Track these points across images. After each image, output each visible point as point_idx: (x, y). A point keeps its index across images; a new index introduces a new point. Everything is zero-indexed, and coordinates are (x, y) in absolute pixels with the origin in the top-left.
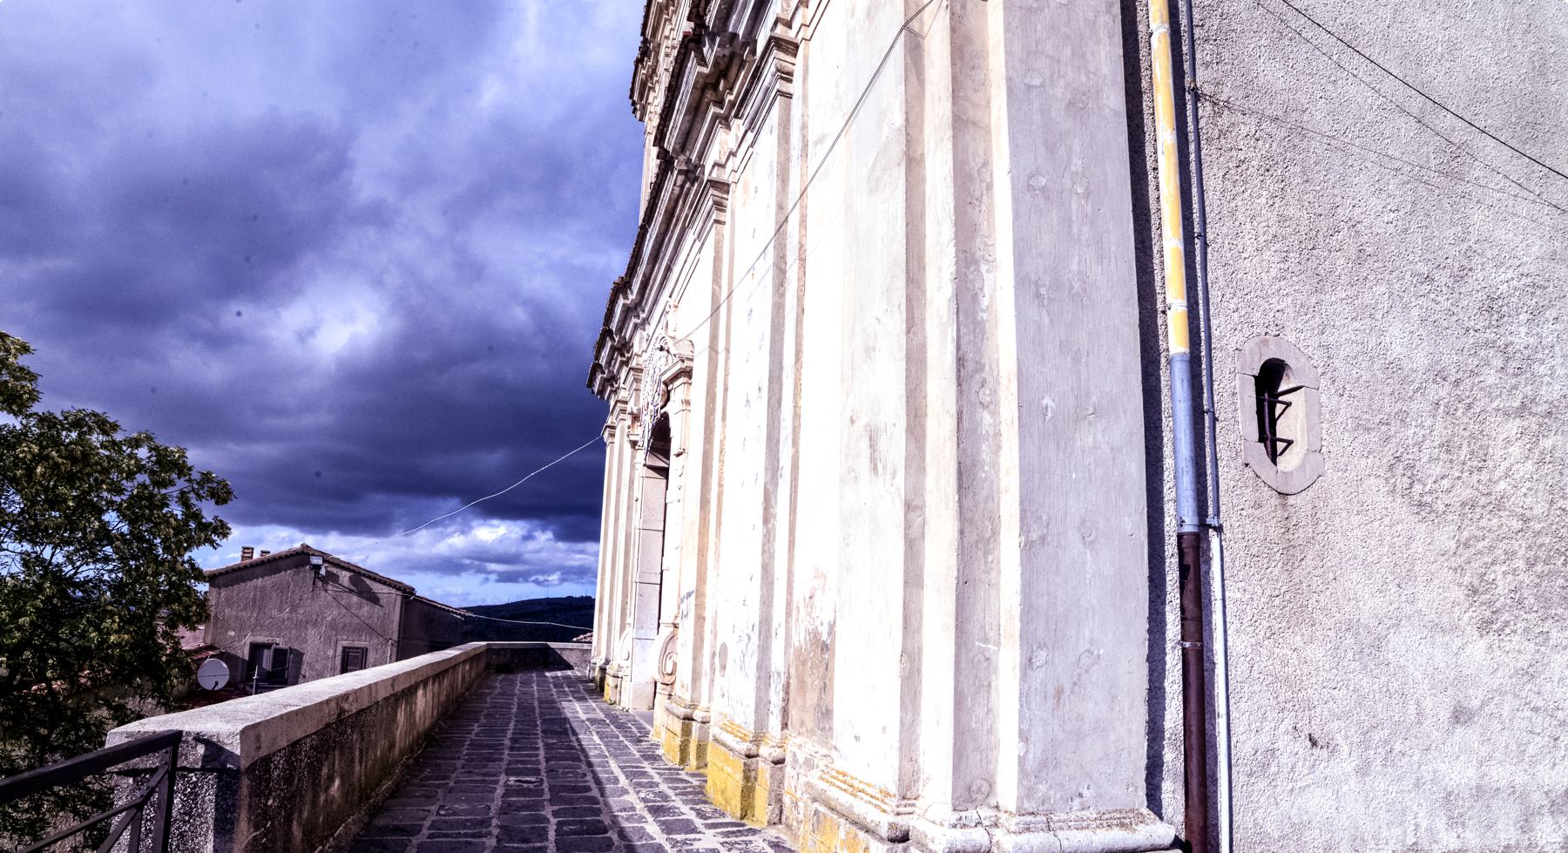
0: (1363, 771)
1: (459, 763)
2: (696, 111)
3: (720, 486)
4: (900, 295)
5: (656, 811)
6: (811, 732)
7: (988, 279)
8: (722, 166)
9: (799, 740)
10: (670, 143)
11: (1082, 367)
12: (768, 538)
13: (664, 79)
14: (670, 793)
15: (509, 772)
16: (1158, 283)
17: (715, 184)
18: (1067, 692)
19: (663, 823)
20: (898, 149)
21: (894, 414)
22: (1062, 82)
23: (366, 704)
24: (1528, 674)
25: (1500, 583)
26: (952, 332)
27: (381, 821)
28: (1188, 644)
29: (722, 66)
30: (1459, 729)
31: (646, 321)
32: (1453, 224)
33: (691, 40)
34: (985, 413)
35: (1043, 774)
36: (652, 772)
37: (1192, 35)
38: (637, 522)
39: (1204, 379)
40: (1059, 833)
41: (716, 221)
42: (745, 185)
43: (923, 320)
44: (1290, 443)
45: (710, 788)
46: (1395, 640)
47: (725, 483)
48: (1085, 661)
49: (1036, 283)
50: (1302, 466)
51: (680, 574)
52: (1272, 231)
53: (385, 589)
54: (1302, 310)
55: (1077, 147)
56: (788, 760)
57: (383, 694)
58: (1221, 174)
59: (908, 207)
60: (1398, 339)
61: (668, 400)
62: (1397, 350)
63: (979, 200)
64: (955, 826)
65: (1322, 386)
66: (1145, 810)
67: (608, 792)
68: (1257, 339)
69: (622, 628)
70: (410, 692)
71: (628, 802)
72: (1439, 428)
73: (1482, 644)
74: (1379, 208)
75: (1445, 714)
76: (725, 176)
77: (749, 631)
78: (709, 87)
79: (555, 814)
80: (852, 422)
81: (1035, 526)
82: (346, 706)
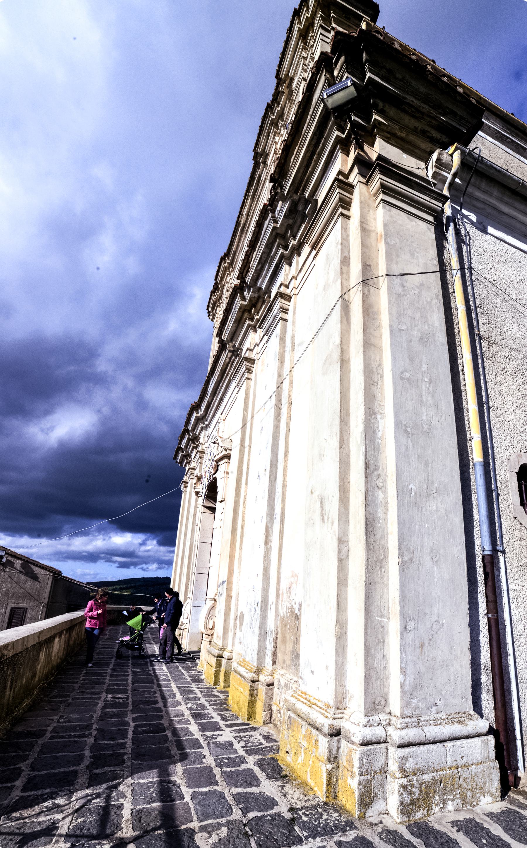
1: (77, 686)
2: (239, 322)
3: (243, 521)
4: (336, 428)
5: (196, 716)
6: (289, 667)
8: (252, 350)
9: (282, 672)
10: (225, 336)
11: (430, 469)
13: (224, 306)
14: (207, 704)
15: (108, 692)
17: (247, 359)
18: (426, 645)
19: (200, 724)
20: (336, 355)
22: (416, 329)
23: (19, 650)
27: (19, 729)
28: (490, 616)
29: (254, 302)
31: (208, 426)
33: (238, 288)
34: (380, 492)
35: (415, 693)
36: (197, 691)
37: (476, 311)
38: (196, 538)
39: (492, 474)
40: (425, 728)
41: (247, 378)
42: (263, 362)
43: (348, 442)
45: (231, 702)
47: (246, 519)
48: (435, 627)
49: (405, 425)
51: (218, 571)
52: (520, 401)
53: (43, 572)
55: (424, 360)
56: (276, 684)
57: (32, 643)
58: (494, 374)
61: (217, 470)
64: (366, 726)
66: (472, 712)
68: (516, 454)
70: (51, 640)
76: (252, 355)
77: (255, 606)
78: (246, 312)
79: (134, 720)
80: (312, 493)
82: (6, 652)
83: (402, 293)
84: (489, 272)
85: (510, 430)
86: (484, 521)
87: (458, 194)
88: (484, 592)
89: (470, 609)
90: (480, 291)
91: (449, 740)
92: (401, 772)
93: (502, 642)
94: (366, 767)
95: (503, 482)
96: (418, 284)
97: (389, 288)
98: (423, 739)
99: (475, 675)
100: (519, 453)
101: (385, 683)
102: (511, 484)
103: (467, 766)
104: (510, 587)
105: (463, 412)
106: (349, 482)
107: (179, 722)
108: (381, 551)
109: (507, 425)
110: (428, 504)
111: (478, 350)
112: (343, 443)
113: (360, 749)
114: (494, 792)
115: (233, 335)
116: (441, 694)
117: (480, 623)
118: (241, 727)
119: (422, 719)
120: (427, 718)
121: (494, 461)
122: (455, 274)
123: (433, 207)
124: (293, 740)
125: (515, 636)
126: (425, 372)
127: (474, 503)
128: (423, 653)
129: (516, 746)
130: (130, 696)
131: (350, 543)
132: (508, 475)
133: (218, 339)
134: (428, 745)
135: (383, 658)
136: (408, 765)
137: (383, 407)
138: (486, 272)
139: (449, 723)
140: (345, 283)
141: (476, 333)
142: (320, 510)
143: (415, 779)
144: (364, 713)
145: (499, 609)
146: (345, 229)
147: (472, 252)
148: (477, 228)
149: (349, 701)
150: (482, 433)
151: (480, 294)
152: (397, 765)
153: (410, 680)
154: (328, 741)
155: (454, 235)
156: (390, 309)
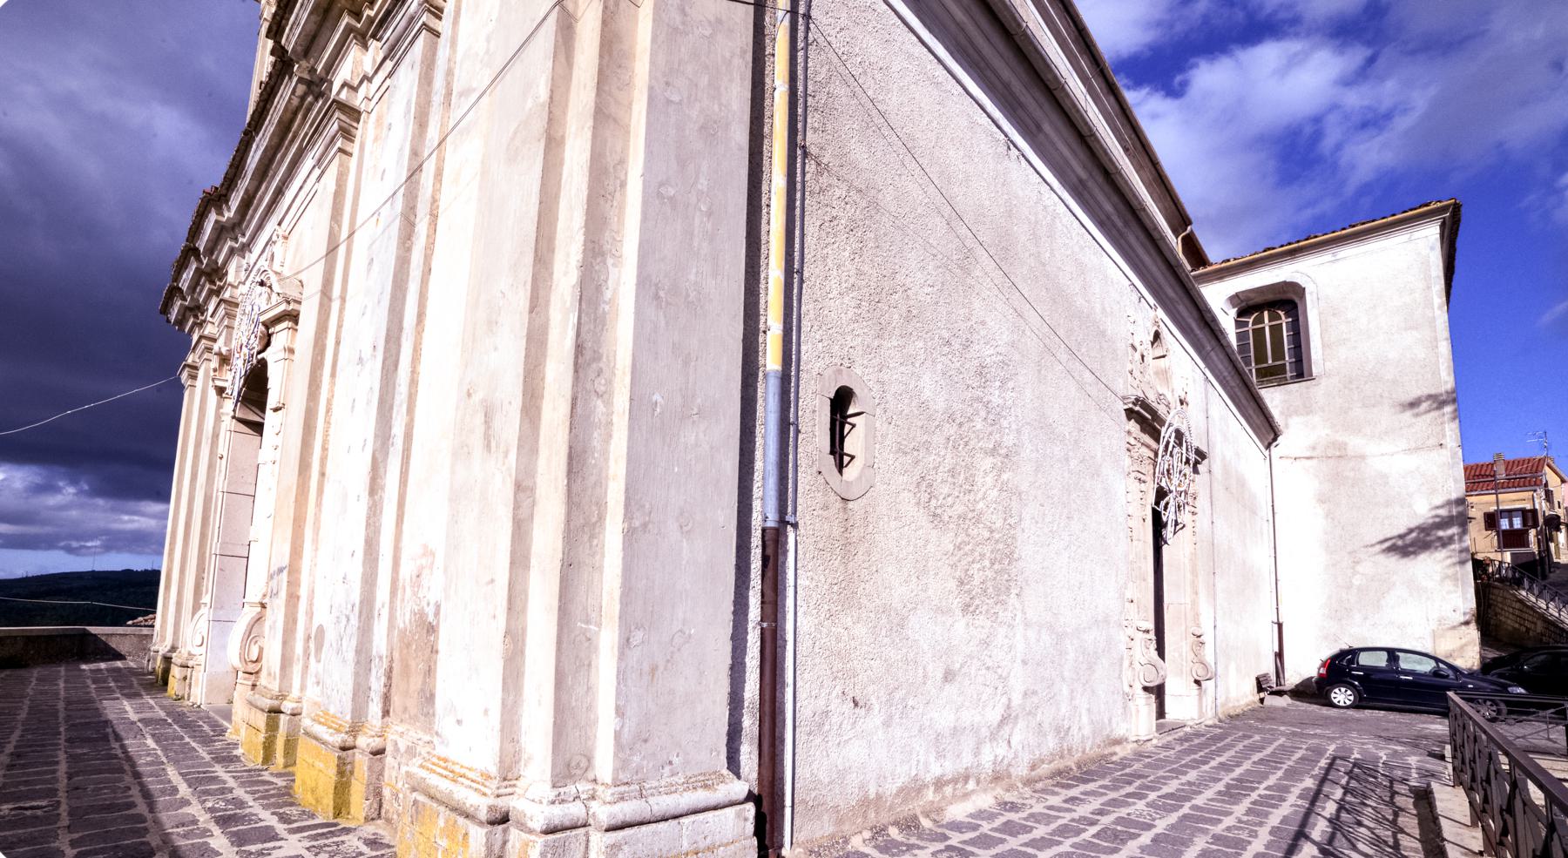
0: (887, 724)
5: (224, 821)
6: (414, 719)
7: (613, 272)
9: (400, 729)
10: (290, 40)
12: (374, 511)
14: (248, 798)
16: (762, 306)
18: (661, 668)
20: (539, 125)
21: (511, 392)
22: (698, 105)
24: (986, 643)
26: (573, 319)
31: (246, 248)
34: (599, 402)
38: (220, 483)
43: (548, 302)
44: (853, 457)
45: (298, 789)
48: (678, 640)
50: (860, 478)
52: (852, 280)
54: (868, 351)
55: (704, 169)
59: (543, 185)
61: (268, 344)
62: (927, 394)
66: (725, 772)
67: (160, 806)
69: (196, 607)
71: (187, 810)
73: (963, 622)
75: (940, 675)
76: (357, 101)
79: (73, 844)
80: (469, 395)
89: (735, 613)
90: (817, 65)
96: (712, 19)
98: (648, 816)
106: (543, 379)
107: (185, 836)
112: (537, 302)
115: (311, 43)
118: (320, 831)
120: (655, 784)
124: (421, 839)
127: (759, 441)
129: (783, 816)
130: (63, 800)
133: (270, 43)
138: (833, 33)
151: (816, 74)
156: (653, 54)
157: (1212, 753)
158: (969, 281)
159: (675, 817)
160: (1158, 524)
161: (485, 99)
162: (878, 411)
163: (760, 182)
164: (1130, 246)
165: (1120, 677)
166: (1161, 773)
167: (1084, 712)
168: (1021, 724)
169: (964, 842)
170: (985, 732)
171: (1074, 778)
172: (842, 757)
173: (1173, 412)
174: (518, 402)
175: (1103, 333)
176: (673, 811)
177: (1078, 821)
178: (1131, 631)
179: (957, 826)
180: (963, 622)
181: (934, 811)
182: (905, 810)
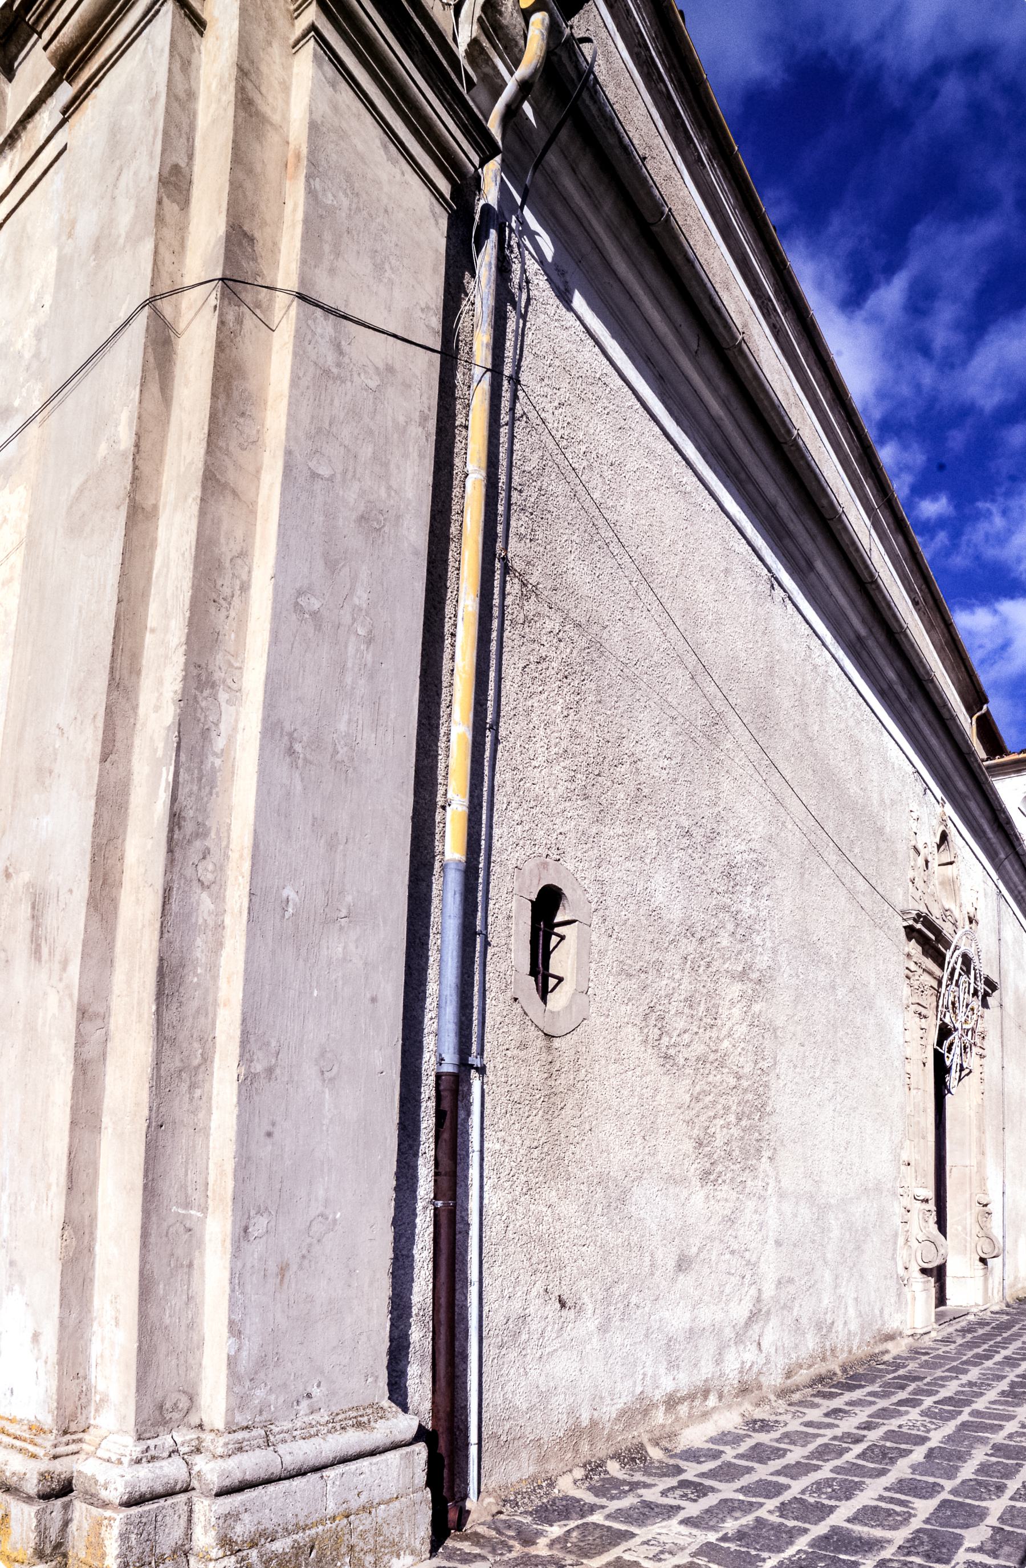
18: (294, 1267)
20: (119, 483)
22: (356, 486)
24: (730, 1220)
25: (718, 1136)
26: (167, 775)
28: (440, 1204)
30: (681, 1277)
32: (709, 786)
34: (204, 896)
35: (261, 1375)
37: (509, 497)
39: (480, 894)
43: (129, 748)
44: (560, 980)
46: (637, 1193)
48: (317, 1228)
49: (290, 735)
50: (569, 1008)
52: (564, 744)
58: (521, 665)
59: (124, 575)
60: (662, 887)
62: (659, 899)
63: (229, 600)
64: (138, 1461)
65: (594, 923)
66: (386, 1403)
68: (538, 860)
72: (685, 981)
74: (657, 751)
75: (671, 1264)
80: (8, 876)
81: (260, 1054)
83: (335, 370)
84: (556, 412)
85: (533, 804)
86: (449, 998)
87: (522, 154)
88: (433, 1153)
90: (527, 450)
91: (332, 1465)
92: (222, 1547)
93: (459, 1258)
94: (137, 1551)
95: (500, 917)
96: (381, 365)
97: (300, 338)
98: (276, 1470)
99: (397, 1328)
100: (543, 858)
101: (191, 1361)
102: (517, 924)
103: (367, 1509)
104: (486, 1145)
105: (436, 738)
106: (121, 859)
108: (196, 1045)
109: (529, 791)
110: (323, 942)
111: (496, 596)
113: (122, 1515)
114: (418, 1546)
116: (322, 1373)
117: (418, 1220)
119: (275, 1429)
120: (287, 1425)
121: (489, 868)
122: (476, 378)
123: (455, 152)
125: (485, 1245)
126: (361, 610)
127: (433, 956)
128: (285, 1286)
129: (467, 1457)
131: (112, 1020)
132: (514, 904)
134: (286, 1482)
135: (187, 1304)
136: (239, 1529)
137: (237, 672)
138: (550, 407)
139: (336, 1430)
140: (167, 262)
141: (498, 552)
142: (29, 925)
143: (254, 1553)
144: (133, 1434)
145: (459, 1191)
146: (182, 62)
147: (527, 341)
148: (550, 280)
149: (97, 1411)
150: (471, 796)
151: (525, 460)
152: (214, 1533)
153: (251, 1348)
154: (38, 1512)
155: (493, 269)
157: (997, 1345)
158: (717, 754)
159: (316, 1469)
160: (941, 1070)
161: (33, 428)
162: (596, 920)
163: (442, 601)
164: (915, 724)
165: (893, 1258)
166: (939, 1373)
167: (850, 1302)
168: (774, 1321)
169: (702, 1475)
170: (729, 1333)
171: (839, 1385)
172: (548, 1378)
173: (960, 932)
174: (82, 891)
175: (880, 831)
176: (313, 1461)
177: (840, 1439)
178: (907, 1201)
179: (693, 1455)
180: (702, 1194)
181: (663, 1438)
182: (626, 1439)
